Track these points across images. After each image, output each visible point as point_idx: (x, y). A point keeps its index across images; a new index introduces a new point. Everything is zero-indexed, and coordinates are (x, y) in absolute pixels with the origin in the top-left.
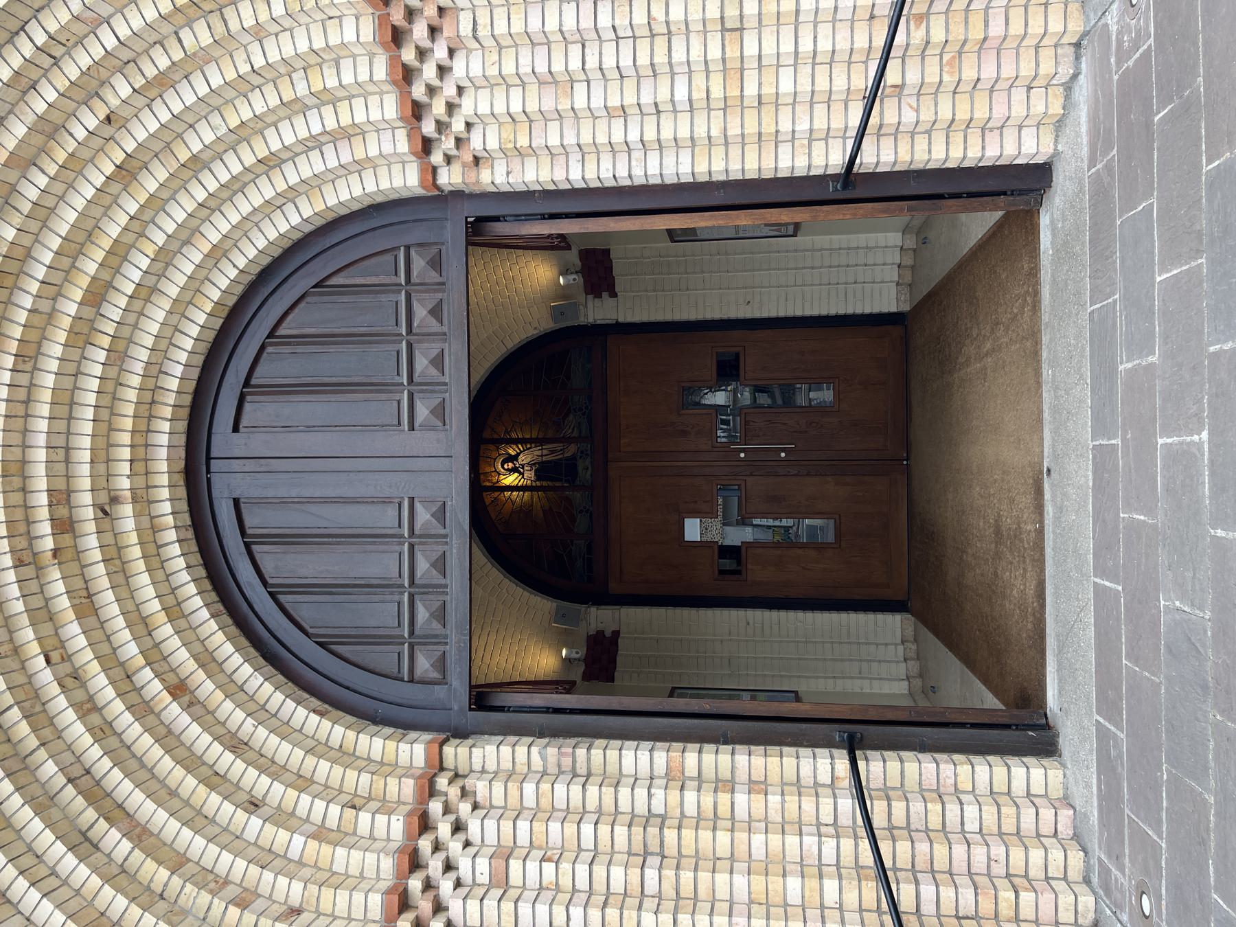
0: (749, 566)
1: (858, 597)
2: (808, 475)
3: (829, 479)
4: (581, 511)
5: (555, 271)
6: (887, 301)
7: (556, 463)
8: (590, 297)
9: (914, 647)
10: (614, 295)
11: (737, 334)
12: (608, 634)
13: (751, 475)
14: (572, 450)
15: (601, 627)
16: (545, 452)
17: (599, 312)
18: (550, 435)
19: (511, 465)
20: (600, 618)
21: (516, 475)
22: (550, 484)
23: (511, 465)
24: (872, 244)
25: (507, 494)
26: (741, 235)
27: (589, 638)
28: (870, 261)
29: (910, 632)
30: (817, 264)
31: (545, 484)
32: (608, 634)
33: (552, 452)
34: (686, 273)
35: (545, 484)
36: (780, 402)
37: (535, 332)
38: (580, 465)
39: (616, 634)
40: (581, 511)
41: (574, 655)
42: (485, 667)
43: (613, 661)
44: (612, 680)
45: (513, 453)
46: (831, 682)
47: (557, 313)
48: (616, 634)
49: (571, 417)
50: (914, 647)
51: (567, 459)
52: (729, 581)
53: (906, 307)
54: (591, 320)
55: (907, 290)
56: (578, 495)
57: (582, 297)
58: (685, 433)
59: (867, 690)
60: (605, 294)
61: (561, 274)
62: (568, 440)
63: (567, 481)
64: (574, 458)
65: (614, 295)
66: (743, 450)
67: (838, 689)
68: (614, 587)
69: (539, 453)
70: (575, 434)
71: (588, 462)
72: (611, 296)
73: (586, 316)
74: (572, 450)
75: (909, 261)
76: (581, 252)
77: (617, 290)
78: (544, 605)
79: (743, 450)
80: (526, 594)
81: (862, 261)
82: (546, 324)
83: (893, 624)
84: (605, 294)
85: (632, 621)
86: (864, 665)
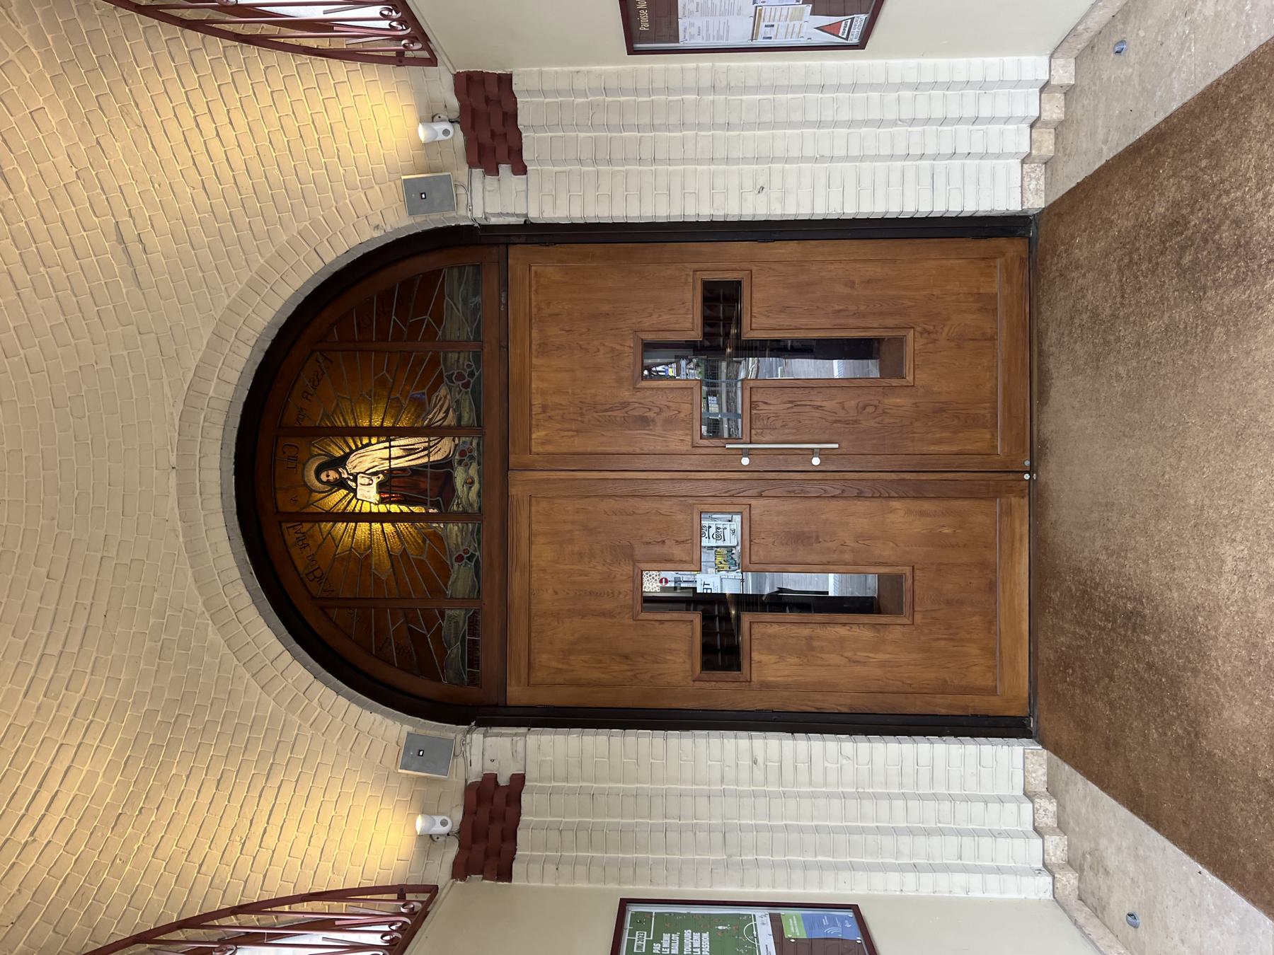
0: (756, 656)
1: (943, 711)
2: (860, 496)
3: (896, 504)
4: (459, 559)
5: (411, 116)
6: (1003, 190)
7: (415, 471)
8: (478, 172)
9: (1052, 807)
10: (520, 169)
11: (738, 249)
12: (503, 780)
13: (760, 496)
14: (444, 448)
15: (491, 768)
16: (396, 452)
17: (492, 200)
18: (403, 423)
19: (333, 475)
20: (490, 751)
21: (343, 492)
22: (405, 509)
23: (333, 475)
24: (993, 76)
25: (326, 526)
26: (760, 42)
27: (469, 788)
28: (985, 112)
29: (1039, 777)
30: (891, 115)
31: (394, 508)
32: (503, 780)
33: (409, 451)
34: (653, 127)
35: (394, 508)
36: (725, 410)
37: (376, 234)
38: (459, 476)
39: (519, 781)
40: (459, 559)
41: (439, 829)
42: (265, 856)
43: (510, 837)
44: (505, 874)
45: (338, 453)
46: (910, 877)
47: (417, 194)
48: (519, 781)
49: (443, 391)
50: (1052, 807)
51: (435, 465)
52: (718, 668)
53: (1036, 202)
54: (478, 214)
55: (1040, 171)
56: (454, 528)
57: (461, 172)
58: (644, 422)
59: (976, 894)
60: (504, 169)
61: (422, 121)
62: (439, 432)
63: (434, 505)
64: (447, 463)
65: (520, 169)
66: (747, 453)
67: (926, 891)
68: (516, 694)
69: (385, 453)
70: (451, 420)
71: (473, 471)
72: (515, 172)
73: (470, 207)
74: (444, 448)
75: (1054, 110)
76: (457, 77)
77: (526, 156)
78: (389, 729)
79: (821, 453)
80: (355, 708)
81: (969, 112)
82: (395, 220)
83: (1008, 763)
84: (504, 169)
85: (546, 758)
86: (968, 841)
